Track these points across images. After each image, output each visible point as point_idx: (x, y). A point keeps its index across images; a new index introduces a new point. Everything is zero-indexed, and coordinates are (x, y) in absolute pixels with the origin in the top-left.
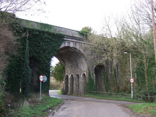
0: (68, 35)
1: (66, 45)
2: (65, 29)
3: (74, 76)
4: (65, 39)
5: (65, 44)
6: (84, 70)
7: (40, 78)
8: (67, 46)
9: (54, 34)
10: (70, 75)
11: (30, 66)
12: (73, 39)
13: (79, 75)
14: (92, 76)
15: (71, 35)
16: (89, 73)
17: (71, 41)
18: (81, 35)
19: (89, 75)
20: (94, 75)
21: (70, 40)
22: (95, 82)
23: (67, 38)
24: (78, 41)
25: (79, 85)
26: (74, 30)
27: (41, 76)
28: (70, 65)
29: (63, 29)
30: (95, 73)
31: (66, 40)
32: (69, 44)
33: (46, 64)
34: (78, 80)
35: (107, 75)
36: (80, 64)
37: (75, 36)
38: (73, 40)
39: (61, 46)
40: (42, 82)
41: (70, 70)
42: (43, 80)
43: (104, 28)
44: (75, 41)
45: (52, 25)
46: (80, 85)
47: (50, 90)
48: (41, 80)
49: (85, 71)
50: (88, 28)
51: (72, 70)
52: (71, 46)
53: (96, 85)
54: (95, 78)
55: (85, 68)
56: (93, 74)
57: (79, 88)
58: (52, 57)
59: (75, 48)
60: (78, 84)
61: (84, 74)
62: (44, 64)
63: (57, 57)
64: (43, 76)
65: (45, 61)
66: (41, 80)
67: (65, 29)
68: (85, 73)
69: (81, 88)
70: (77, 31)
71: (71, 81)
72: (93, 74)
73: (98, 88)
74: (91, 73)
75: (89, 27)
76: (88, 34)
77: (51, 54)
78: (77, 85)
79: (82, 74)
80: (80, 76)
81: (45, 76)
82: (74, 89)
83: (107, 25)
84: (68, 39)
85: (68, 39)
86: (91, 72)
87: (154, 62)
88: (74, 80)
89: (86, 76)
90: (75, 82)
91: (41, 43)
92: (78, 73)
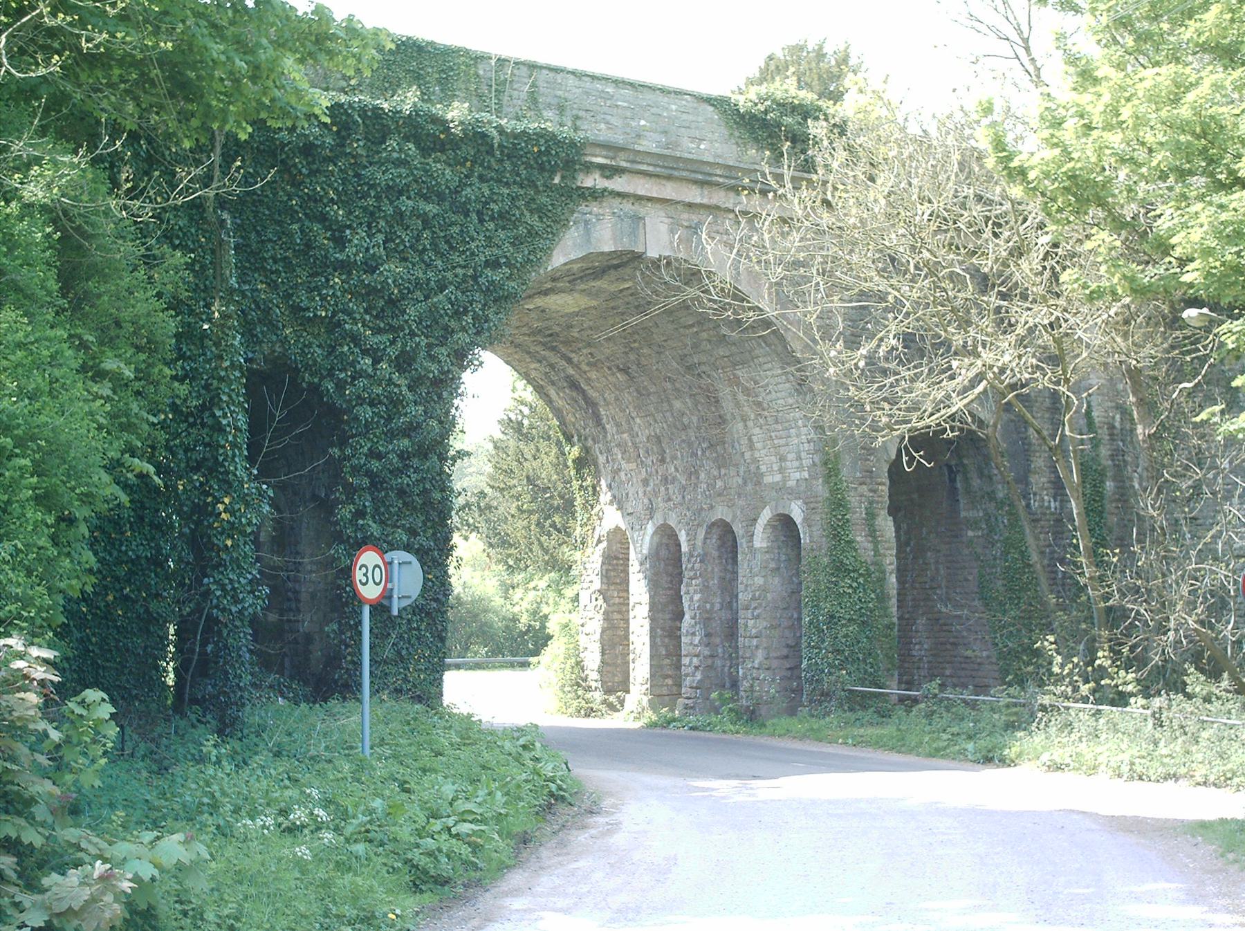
0: (619, 139)
1: (606, 238)
2: (587, 84)
3: (683, 537)
4: (591, 181)
5: (588, 232)
6: (784, 480)
7: (359, 575)
8: (608, 248)
9: (484, 136)
10: (650, 528)
11: (251, 459)
12: (669, 178)
13: (738, 529)
14: (860, 538)
15: (649, 144)
16: (838, 504)
17: (650, 199)
18: (756, 140)
19: (838, 533)
20: (887, 526)
21: (642, 187)
22: (894, 601)
23: (610, 171)
24: (719, 198)
25: (732, 631)
26: (678, 93)
27: (369, 557)
28: (642, 429)
29: (571, 80)
30: (893, 511)
31: (595, 195)
32: (633, 234)
33: (411, 430)
34: (722, 579)
35: (1014, 523)
36: (744, 420)
37: (688, 148)
38: (668, 190)
39: (548, 251)
40: (380, 608)
41: (645, 482)
42: (387, 595)
43: (974, 60)
44: (694, 195)
45: (459, 50)
46: (751, 624)
47: (449, 667)
48: (370, 592)
49: (794, 494)
50: (820, 55)
51: (665, 480)
52: (652, 253)
53: (906, 622)
54: (890, 561)
55: (791, 464)
56: (871, 516)
57: (734, 658)
58: (461, 358)
59: (693, 276)
60: (725, 615)
61: (785, 524)
62: (391, 435)
63: (518, 356)
64: (382, 553)
65: (396, 403)
66: (370, 592)
67: (594, 78)
68: (797, 514)
69: (760, 655)
70: (709, 100)
71: (654, 585)
72: (871, 516)
73: (922, 648)
74: (858, 513)
75: (828, 49)
76: (817, 129)
77: (462, 338)
78: (716, 625)
79: (766, 515)
80: (742, 543)
81: (398, 556)
82: (685, 661)
83: (1014, 36)
84: (618, 184)
85: (618, 184)
86: (853, 500)
87: (1125, 778)
88: (687, 574)
89: (805, 539)
90: (691, 598)
91: (358, 239)
92: (721, 512)
